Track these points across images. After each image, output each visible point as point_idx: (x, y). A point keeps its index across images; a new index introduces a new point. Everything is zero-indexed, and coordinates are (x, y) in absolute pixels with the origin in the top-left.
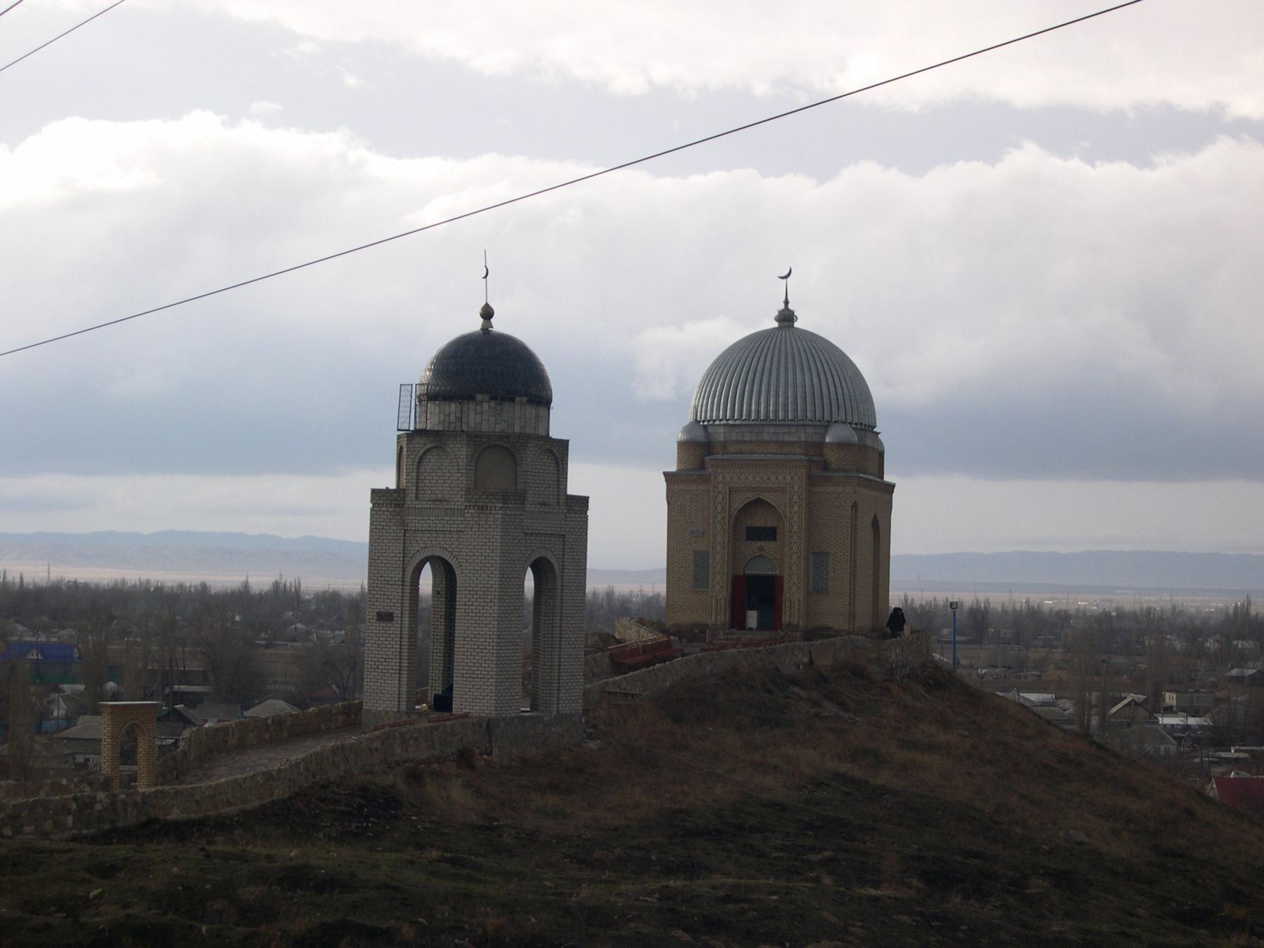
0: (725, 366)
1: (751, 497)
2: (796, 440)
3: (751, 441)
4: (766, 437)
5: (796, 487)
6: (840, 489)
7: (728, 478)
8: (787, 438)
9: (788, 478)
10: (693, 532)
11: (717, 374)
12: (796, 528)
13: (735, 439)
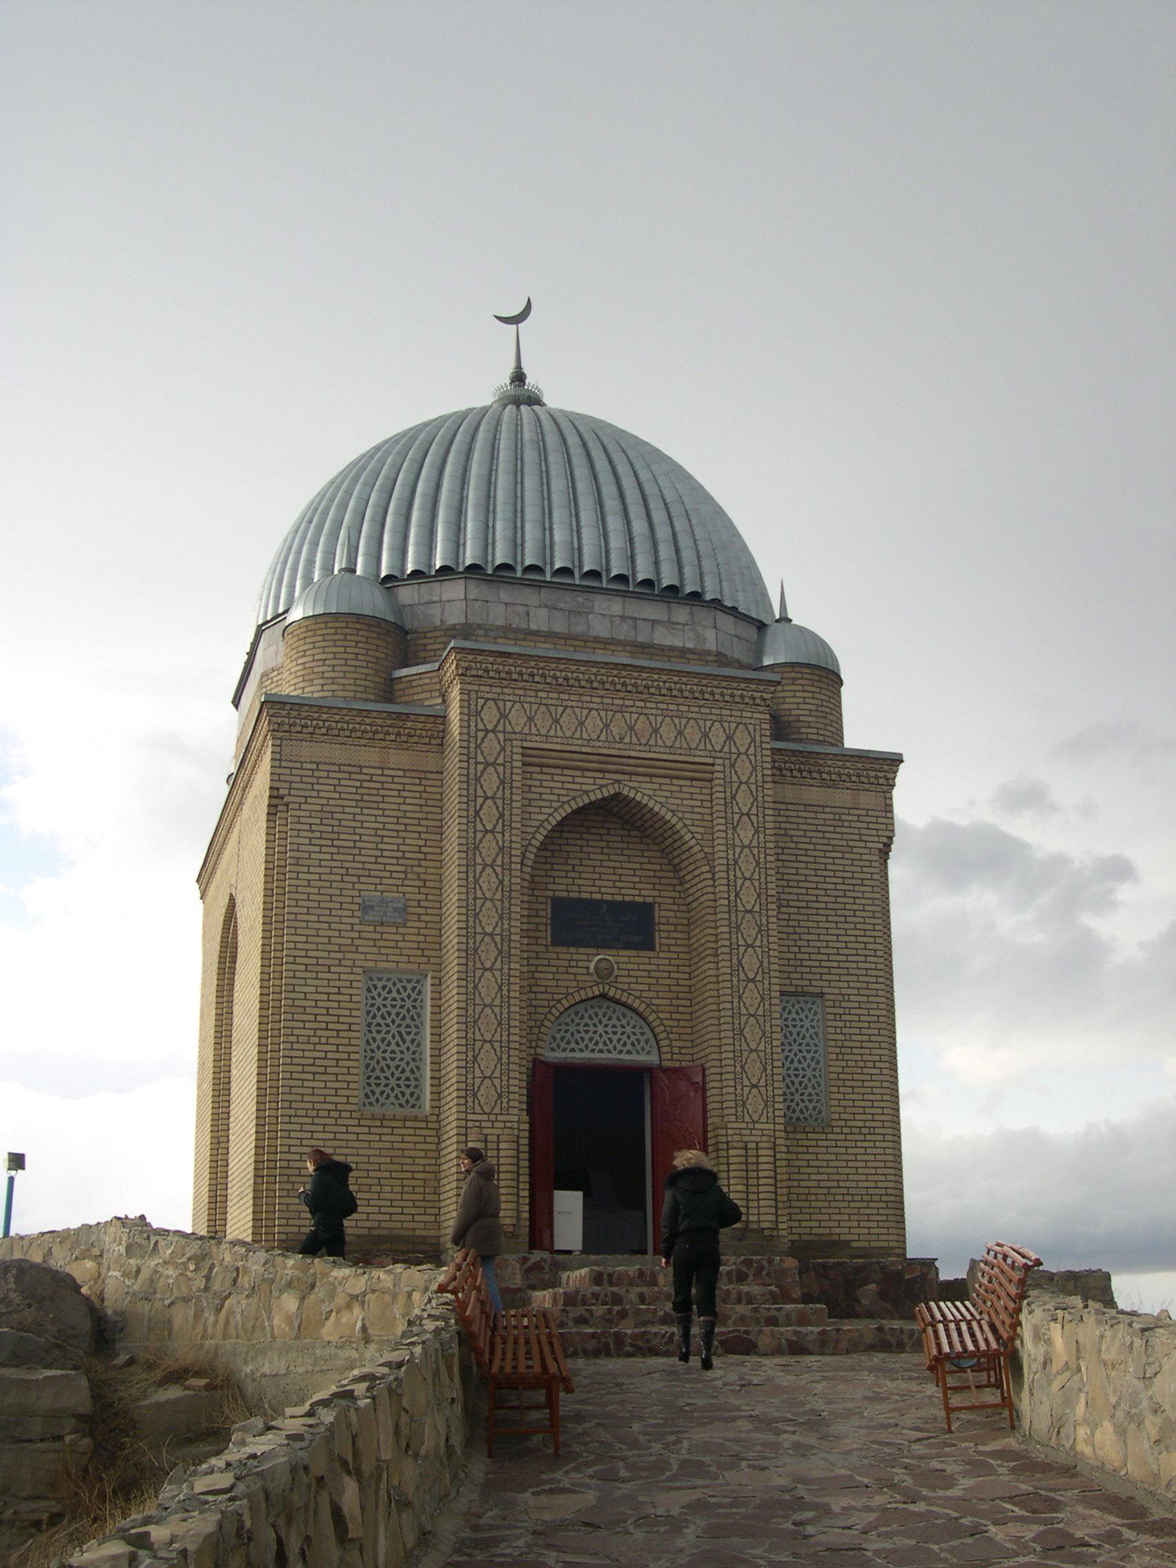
0: (334, 535)
1: (595, 788)
2: (690, 645)
3: (551, 636)
4: (600, 628)
5: (744, 768)
6: (842, 797)
7: (517, 719)
8: (664, 637)
9: (717, 736)
10: (365, 908)
11: (338, 524)
12: (749, 898)
13: (500, 622)
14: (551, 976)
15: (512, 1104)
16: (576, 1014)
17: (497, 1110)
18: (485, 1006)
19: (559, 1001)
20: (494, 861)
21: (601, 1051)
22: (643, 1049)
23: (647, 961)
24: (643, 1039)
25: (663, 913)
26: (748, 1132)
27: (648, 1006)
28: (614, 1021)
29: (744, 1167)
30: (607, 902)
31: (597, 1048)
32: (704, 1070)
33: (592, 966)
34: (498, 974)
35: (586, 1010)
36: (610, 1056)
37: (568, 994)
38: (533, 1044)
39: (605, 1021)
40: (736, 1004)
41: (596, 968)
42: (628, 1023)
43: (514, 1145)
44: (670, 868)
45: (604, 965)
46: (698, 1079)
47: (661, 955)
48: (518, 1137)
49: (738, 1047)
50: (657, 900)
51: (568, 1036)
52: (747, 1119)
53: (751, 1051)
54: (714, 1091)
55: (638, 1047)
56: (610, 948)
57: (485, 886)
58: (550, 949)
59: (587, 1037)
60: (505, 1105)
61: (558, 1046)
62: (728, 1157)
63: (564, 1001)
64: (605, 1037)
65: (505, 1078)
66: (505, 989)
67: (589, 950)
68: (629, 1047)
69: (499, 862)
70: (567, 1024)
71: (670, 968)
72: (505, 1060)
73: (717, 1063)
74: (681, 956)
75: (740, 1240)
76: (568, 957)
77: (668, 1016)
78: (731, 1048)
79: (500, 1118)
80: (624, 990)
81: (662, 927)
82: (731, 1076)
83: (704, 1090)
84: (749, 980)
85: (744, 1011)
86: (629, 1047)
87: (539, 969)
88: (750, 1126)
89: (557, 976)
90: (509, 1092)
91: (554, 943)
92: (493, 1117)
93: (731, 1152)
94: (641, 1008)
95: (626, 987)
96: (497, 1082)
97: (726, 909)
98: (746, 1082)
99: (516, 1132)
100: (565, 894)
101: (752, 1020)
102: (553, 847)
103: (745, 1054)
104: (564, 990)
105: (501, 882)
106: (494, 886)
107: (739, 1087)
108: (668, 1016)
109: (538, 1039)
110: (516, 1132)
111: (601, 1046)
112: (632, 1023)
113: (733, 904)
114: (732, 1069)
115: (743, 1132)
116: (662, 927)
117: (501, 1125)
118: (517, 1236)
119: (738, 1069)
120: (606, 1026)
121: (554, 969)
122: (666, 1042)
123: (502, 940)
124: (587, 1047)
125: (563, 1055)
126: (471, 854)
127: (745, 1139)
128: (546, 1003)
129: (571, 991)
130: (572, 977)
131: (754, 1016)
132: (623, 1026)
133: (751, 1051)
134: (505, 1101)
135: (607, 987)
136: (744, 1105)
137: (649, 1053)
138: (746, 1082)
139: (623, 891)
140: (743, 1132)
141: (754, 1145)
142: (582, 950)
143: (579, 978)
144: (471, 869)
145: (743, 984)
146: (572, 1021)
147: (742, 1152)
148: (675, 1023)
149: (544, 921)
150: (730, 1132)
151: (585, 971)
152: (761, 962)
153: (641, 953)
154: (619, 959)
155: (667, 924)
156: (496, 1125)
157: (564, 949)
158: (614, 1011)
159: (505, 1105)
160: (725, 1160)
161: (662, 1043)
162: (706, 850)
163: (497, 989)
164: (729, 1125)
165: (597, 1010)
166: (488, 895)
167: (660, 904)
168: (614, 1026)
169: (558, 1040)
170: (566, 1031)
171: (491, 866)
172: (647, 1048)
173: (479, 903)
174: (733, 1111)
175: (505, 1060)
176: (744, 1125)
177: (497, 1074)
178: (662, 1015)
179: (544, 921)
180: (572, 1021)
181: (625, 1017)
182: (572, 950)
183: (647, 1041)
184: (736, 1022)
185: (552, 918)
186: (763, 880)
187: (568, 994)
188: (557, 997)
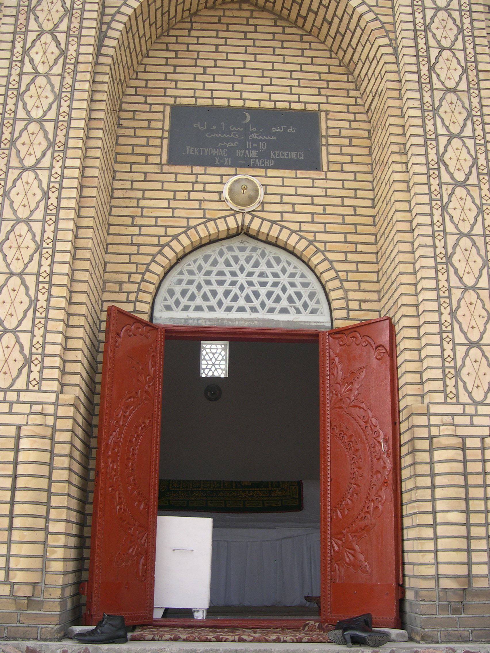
14: (165, 204)
15: (47, 373)
16: (206, 258)
17: (21, 383)
18: (18, 221)
19: (175, 237)
20: (56, 26)
21: (241, 309)
22: (305, 306)
23: (309, 183)
24: (305, 292)
25: (331, 123)
26: (466, 420)
27: (311, 242)
28: (263, 268)
29: (460, 480)
30: (250, 110)
31: (236, 305)
32: (392, 327)
33: (226, 189)
34: (44, 175)
35: (221, 254)
36: (254, 315)
37: (188, 228)
38: (132, 297)
39: (248, 268)
40: (437, 217)
41: (231, 191)
42: (284, 271)
43: (46, 444)
44: (341, 70)
45: (238, 188)
46: (385, 339)
47: (330, 175)
48: (54, 429)
49: (443, 283)
50: (323, 107)
51: (193, 288)
52: (464, 398)
53: (466, 288)
54: (407, 355)
55: (299, 304)
56: (255, 166)
57: (37, 59)
58: (166, 168)
59: (220, 290)
60: (35, 375)
61: (177, 303)
62: (431, 463)
63: (183, 238)
64: (248, 290)
65: (39, 333)
66: (53, 196)
67: (222, 170)
68: (284, 303)
69: (63, 26)
70: (191, 273)
71: (343, 193)
72: (42, 303)
73: (412, 311)
74: (359, 177)
75: (456, 611)
76: (192, 178)
77: (341, 257)
78: (432, 284)
79: (24, 397)
80: (273, 222)
81: (331, 141)
82: (435, 328)
83: (392, 355)
84: (457, 184)
85: (450, 228)
86: (284, 303)
87: (148, 194)
88: (470, 410)
89: (173, 204)
90: (44, 355)
91: (172, 161)
92: (12, 396)
93: (438, 455)
94: (301, 246)
95: (277, 217)
96: (25, 339)
97: (416, 86)
98: (460, 338)
99: (50, 421)
100: (192, 101)
101: (465, 242)
102: (177, 47)
103: (457, 294)
104: (184, 223)
105: (64, 53)
106: (52, 58)
107: (448, 347)
108: (341, 257)
109: (139, 290)
110: (50, 421)
111: (241, 302)
112: (290, 270)
113: (425, 80)
114: (435, 317)
115: (458, 420)
116: (331, 141)
117: (25, 408)
118: (40, 604)
119: (446, 317)
120: (250, 274)
121: (170, 195)
122: (339, 293)
123: (56, 128)
124: (220, 304)
125: (184, 315)
126: (22, 19)
127: (461, 431)
128: (155, 240)
129: (193, 223)
130: (196, 205)
131: (468, 235)
132: (275, 275)
133: (466, 288)
134: (35, 369)
135: (248, 218)
136: (457, 375)
137: (314, 312)
138: (460, 338)
139: (274, 97)
140: (458, 420)
141: (477, 443)
142: (211, 170)
143: (206, 205)
144: (19, 39)
145: (446, 190)
146: (200, 268)
147: (458, 455)
148: (353, 267)
149: (159, 133)
150: (434, 420)
151: (216, 197)
152: (475, 159)
153: (300, 173)
154: (266, 181)
155: (340, 136)
156: (17, 408)
157: (187, 169)
158: (263, 255)
159: (35, 375)
160: (426, 469)
161: (333, 295)
162: (383, 18)
163: (39, 194)
164: (433, 409)
165: (237, 253)
166: (42, 69)
167: (327, 112)
168: (262, 275)
169: (178, 295)
170: (190, 282)
171: (51, 32)
172: (312, 305)
173: (26, 80)
174: (439, 385)
175: (42, 303)
176: (459, 409)
177: (27, 325)
178: (331, 256)
179: (159, 133)
180: (200, 268)
181: (278, 260)
182: (197, 169)
183: (312, 295)
184: (440, 244)
185: (171, 131)
186: (470, 49)
187: (188, 228)
188: (171, 231)
